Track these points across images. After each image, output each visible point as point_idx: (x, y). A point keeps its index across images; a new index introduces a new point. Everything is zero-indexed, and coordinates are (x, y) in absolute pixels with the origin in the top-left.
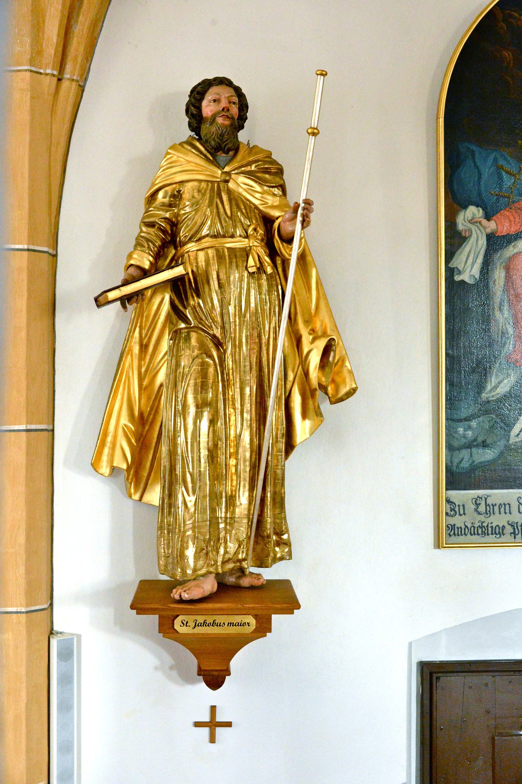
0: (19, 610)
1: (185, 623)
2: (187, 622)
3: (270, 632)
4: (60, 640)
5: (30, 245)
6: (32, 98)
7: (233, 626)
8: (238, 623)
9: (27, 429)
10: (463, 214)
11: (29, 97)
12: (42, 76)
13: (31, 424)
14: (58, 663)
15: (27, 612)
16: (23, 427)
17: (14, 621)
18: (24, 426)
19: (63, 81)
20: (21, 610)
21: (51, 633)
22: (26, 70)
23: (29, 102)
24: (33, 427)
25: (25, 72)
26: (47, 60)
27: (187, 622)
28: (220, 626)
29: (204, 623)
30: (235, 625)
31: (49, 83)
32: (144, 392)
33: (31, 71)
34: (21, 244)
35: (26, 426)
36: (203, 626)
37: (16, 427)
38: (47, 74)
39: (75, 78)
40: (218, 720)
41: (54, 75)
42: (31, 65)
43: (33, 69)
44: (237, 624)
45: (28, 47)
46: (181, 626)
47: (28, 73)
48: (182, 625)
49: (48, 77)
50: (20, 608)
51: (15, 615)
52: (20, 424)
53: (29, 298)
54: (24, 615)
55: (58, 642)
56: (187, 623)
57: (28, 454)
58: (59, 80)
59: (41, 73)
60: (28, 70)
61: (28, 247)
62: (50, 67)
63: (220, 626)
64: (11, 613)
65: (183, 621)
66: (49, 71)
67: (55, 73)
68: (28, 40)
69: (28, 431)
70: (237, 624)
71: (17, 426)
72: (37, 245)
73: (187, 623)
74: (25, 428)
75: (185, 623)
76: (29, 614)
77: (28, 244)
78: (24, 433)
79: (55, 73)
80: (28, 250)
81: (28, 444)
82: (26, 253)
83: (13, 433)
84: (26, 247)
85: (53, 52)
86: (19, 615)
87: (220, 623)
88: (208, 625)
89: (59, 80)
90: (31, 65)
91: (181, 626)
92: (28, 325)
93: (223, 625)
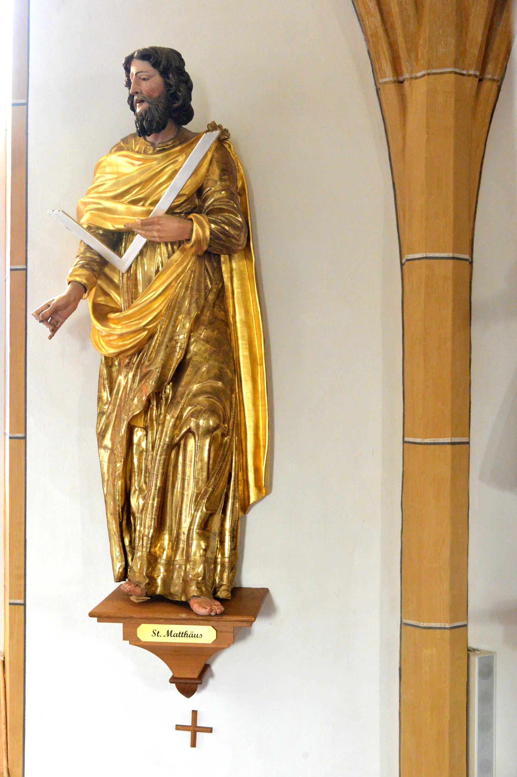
0: (443, 626)
1: (156, 633)
2: (158, 632)
3: (98, 621)
4: (480, 657)
5: (427, 252)
6: (456, 101)
7: (187, 637)
8: (177, 634)
9: (451, 442)
10: (180, 193)
11: (453, 100)
12: (464, 77)
13: (455, 436)
14: (479, 680)
15: (451, 628)
16: (448, 440)
17: (438, 637)
18: (449, 439)
19: (484, 81)
20: (445, 625)
21: (468, 650)
22: (450, 73)
23: (453, 105)
24: (457, 440)
25: (449, 75)
26: (471, 61)
27: (158, 632)
28: (197, 637)
29: (185, 634)
30: (189, 636)
31: (471, 84)
32: (205, 397)
33: (456, 73)
34: (446, 252)
35: (451, 439)
36: (184, 636)
37: (441, 440)
38: (469, 75)
39: (496, 78)
40: (199, 734)
41: (476, 76)
42: (455, 67)
43: (458, 71)
44: (175, 635)
45: (452, 49)
46: (152, 636)
47: (453, 76)
48: (154, 635)
49: (471, 78)
50: (444, 624)
51: (439, 631)
52: (445, 437)
53: (454, 307)
54: (448, 631)
55: (480, 659)
56: (158, 633)
57: (452, 468)
58: (480, 80)
59: (463, 75)
60: (452, 72)
61: (453, 255)
62: (473, 67)
63: (197, 637)
64: (435, 628)
65: (155, 631)
66: (472, 72)
67: (478, 73)
68: (452, 41)
69: (453, 444)
70: (175, 635)
71: (441, 439)
72: (461, 253)
73: (158, 633)
74: (450, 441)
75: (156, 633)
76: (453, 630)
77: (454, 252)
78: (449, 447)
79: (478, 73)
80: (453, 258)
81: (453, 456)
82: (451, 262)
83: (437, 446)
84: (451, 255)
85: (476, 52)
86: (443, 630)
87: (198, 635)
88: (189, 636)
89: (480, 80)
90: (455, 67)
91: (152, 636)
92: (453, 337)
93: (201, 636)
